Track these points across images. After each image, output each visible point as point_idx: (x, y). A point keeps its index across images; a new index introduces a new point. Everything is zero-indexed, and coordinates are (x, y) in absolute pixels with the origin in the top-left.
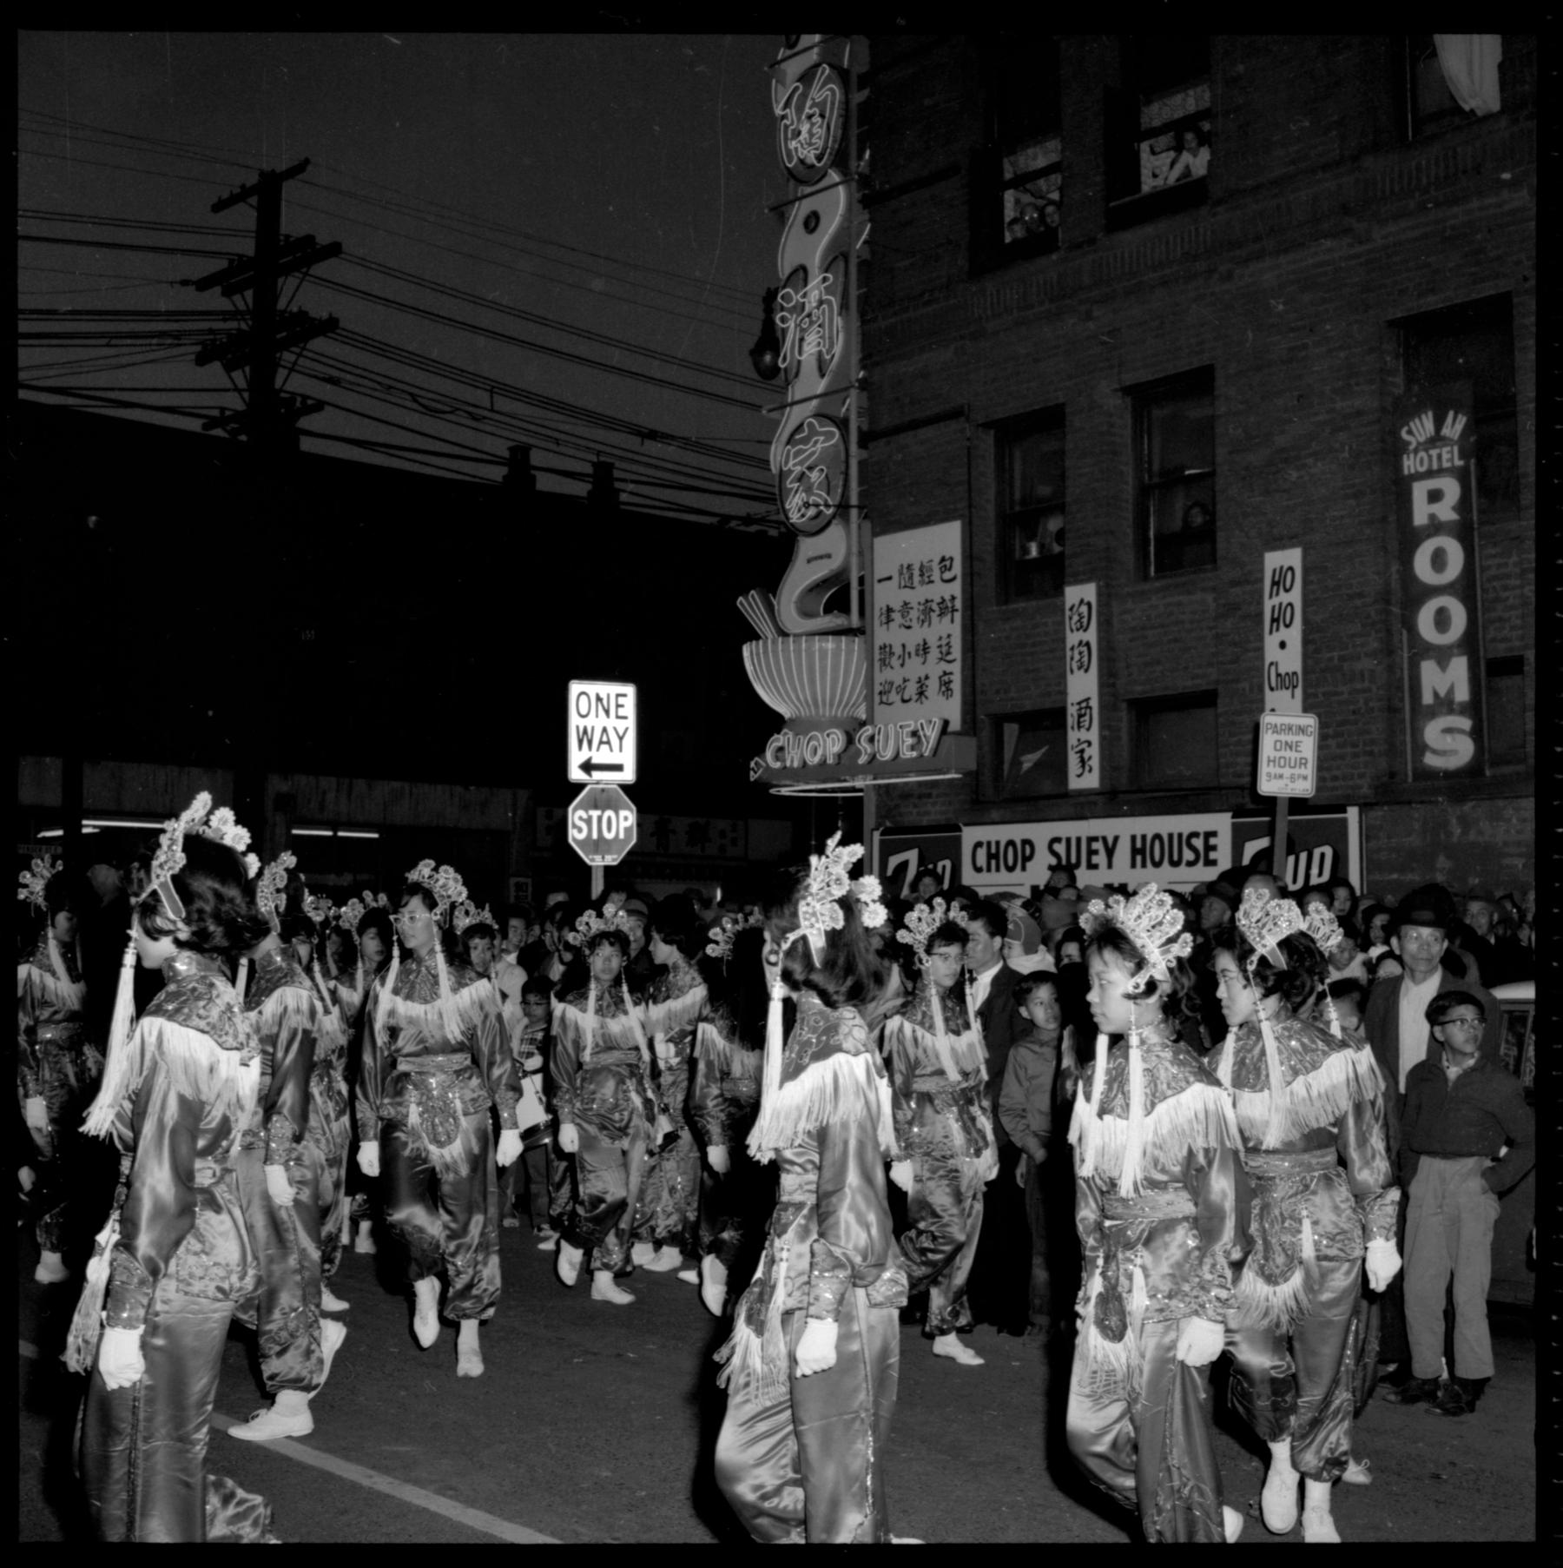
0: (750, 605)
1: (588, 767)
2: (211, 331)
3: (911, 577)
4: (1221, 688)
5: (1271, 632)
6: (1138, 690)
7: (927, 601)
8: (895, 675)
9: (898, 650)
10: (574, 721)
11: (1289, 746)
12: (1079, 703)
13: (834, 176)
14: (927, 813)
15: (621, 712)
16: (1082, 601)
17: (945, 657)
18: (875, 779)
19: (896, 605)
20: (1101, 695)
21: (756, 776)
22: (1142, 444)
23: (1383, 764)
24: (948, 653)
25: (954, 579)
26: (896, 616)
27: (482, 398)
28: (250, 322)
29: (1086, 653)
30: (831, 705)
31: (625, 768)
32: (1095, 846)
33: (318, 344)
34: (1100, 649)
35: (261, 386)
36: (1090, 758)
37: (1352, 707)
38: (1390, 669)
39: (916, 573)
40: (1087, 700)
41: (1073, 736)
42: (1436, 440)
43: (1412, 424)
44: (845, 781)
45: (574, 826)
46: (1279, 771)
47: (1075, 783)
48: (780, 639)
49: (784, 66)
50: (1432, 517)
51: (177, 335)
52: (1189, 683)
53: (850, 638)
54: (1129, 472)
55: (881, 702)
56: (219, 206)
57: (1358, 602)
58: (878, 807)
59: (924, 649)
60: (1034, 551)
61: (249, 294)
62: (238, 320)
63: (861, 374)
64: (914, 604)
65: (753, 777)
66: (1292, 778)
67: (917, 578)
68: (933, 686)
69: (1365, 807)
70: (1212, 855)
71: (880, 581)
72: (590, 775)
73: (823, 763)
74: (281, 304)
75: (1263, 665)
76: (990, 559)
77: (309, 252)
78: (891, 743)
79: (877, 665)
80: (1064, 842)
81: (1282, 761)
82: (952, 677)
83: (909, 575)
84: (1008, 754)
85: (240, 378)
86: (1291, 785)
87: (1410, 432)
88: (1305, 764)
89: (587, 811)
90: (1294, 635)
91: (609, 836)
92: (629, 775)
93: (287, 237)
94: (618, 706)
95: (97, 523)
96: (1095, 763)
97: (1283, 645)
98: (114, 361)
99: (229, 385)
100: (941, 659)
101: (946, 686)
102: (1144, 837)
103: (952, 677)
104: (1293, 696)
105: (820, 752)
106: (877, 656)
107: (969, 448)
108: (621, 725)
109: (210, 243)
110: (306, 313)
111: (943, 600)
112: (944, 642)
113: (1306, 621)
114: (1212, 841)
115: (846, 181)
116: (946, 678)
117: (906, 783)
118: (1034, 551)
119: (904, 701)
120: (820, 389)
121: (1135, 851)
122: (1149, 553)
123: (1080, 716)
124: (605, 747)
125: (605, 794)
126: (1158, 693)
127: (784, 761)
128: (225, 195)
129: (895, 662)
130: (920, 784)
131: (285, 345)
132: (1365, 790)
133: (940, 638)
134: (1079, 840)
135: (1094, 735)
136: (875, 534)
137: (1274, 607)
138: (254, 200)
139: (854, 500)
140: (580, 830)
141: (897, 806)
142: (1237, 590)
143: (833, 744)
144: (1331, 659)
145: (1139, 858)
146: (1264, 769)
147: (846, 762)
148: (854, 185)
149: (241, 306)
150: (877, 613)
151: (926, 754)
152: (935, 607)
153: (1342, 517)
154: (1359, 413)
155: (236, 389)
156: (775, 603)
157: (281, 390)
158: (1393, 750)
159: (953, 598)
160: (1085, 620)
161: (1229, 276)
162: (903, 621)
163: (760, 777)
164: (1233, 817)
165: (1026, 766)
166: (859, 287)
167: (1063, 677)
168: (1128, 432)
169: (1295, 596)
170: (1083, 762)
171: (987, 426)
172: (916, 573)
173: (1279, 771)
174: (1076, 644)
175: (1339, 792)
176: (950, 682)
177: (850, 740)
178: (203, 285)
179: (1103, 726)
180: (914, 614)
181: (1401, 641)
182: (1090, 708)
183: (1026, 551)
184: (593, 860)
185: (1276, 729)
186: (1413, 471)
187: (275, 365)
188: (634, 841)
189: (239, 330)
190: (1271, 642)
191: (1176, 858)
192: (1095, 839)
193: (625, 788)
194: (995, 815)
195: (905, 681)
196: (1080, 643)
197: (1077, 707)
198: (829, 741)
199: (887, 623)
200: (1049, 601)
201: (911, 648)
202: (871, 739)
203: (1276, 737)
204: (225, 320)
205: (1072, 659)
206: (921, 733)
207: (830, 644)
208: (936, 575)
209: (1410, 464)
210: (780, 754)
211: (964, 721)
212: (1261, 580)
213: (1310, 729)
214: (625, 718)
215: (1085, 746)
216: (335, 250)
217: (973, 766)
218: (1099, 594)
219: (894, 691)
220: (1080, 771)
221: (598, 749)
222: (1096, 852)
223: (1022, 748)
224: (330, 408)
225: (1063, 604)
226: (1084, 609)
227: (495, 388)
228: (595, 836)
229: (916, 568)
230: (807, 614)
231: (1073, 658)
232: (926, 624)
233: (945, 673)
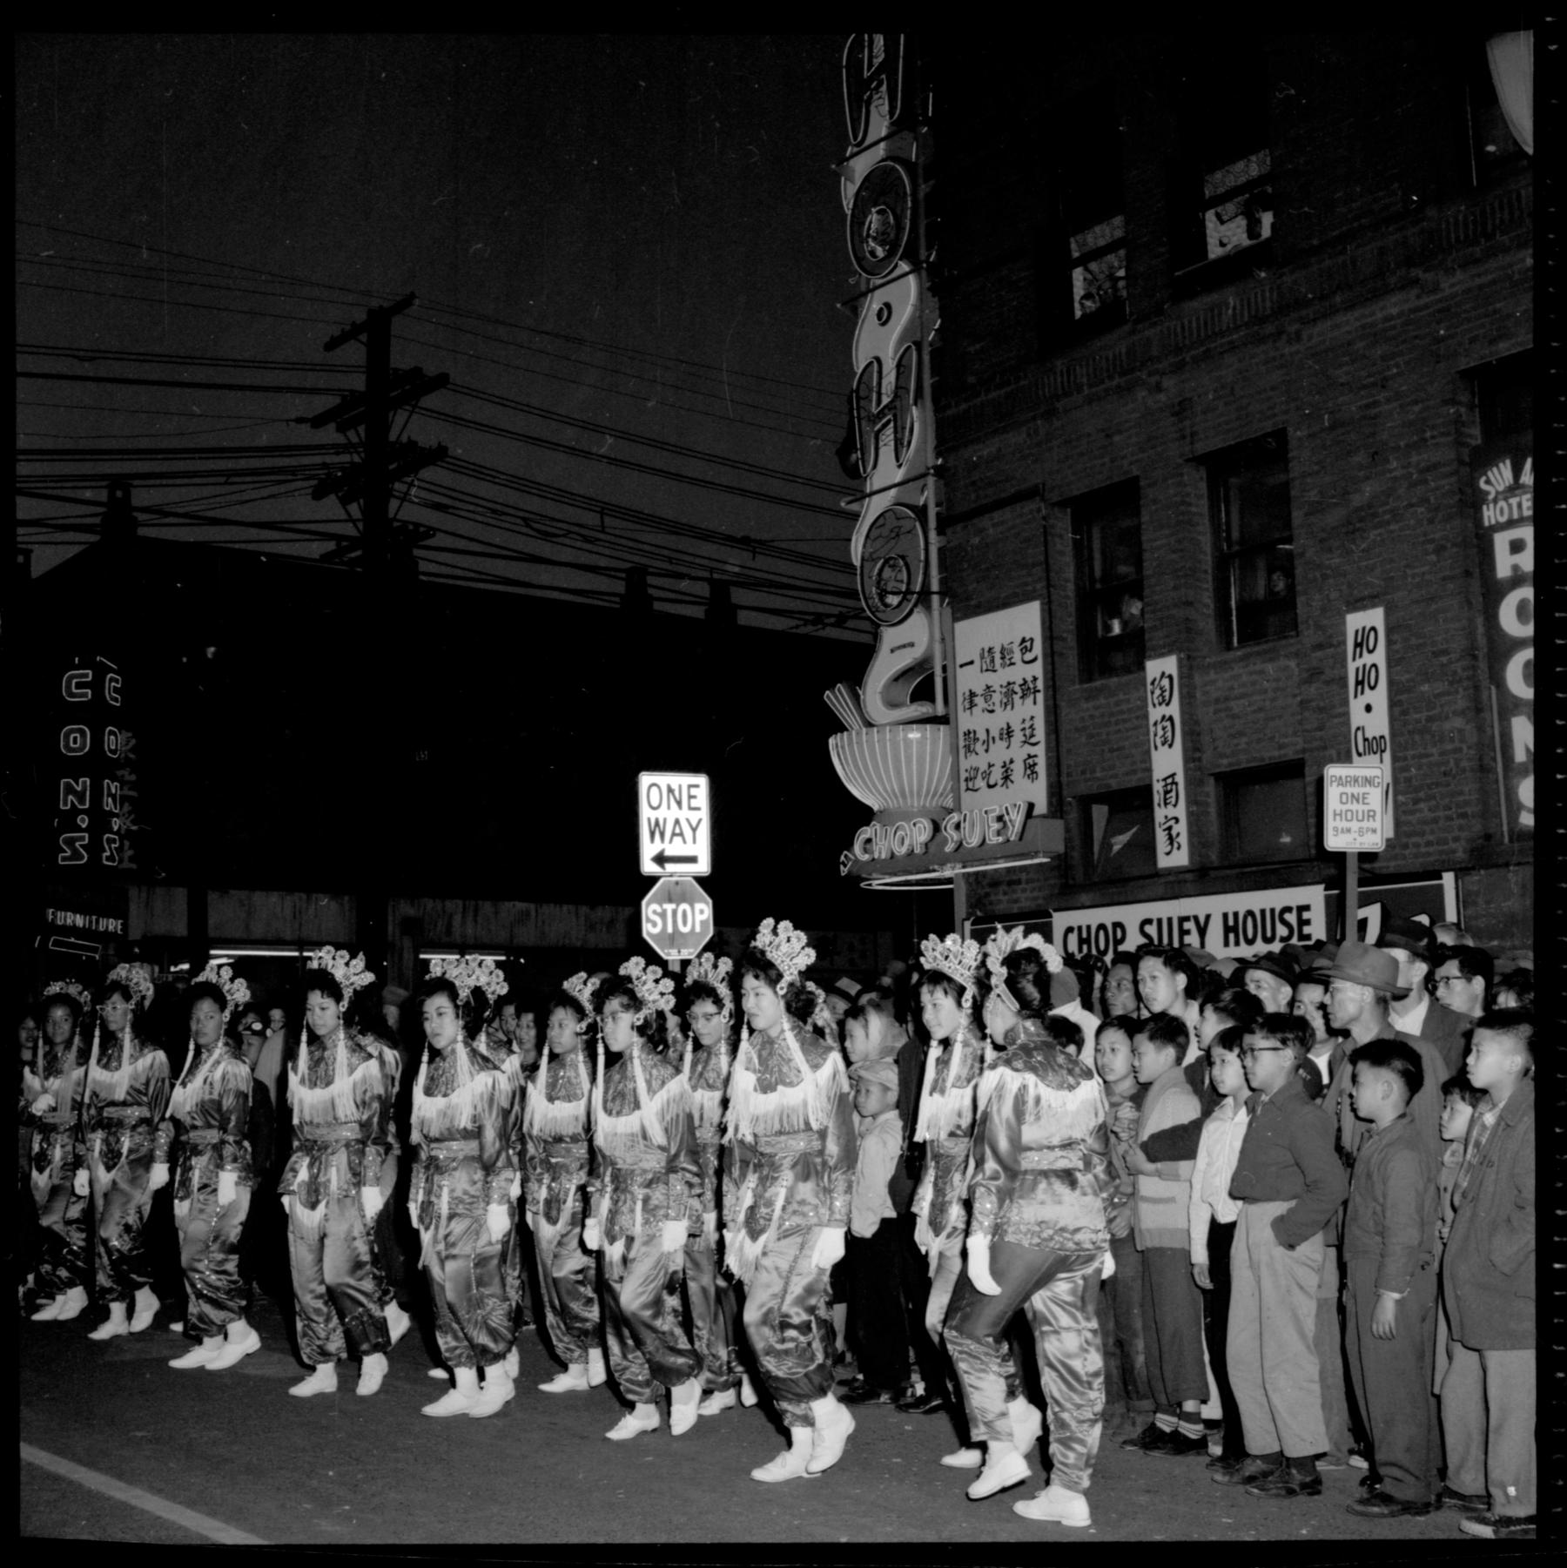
0: (837, 699)
1: (660, 859)
2: (324, 465)
3: (993, 661)
4: (1307, 756)
5: (1356, 696)
6: (1224, 765)
7: (1009, 684)
8: (980, 761)
9: (982, 736)
10: (646, 814)
11: (1355, 798)
12: (1165, 780)
13: (904, 267)
14: (1016, 901)
15: (694, 803)
16: (1163, 674)
17: (1028, 740)
18: (964, 867)
19: (979, 690)
20: (1186, 770)
21: (846, 870)
22: (1220, 511)
23: (1477, 827)
24: (1032, 736)
25: (1035, 660)
26: (979, 700)
27: (592, 519)
28: (363, 455)
29: (1169, 728)
30: (919, 795)
31: (700, 859)
32: (1187, 925)
33: (427, 473)
34: (1183, 723)
35: (375, 515)
36: (1178, 835)
37: (1443, 769)
38: (1480, 729)
39: (997, 656)
40: (1173, 775)
41: (1160, 814)
42: (1515, 488)
43: (1490, 474)
44: (934, 871)
45: (648, 920)
46: (1345, 824)
47: (1164, 862)
48: (864, 730)
49: (852, 162)
50: (1515, 568)
51: (293, 471)
52: (1276, 753)
53: (936, 726)
54: (1206, 541)
55: (968, 789)
56: (332, 345)
57: (1444, 659)
58: (968, 897)
59: (1008, 733)
60: (1117, 628)
61: (362, 429)
62: (351, 453)
63: (940, 461)
64: (996, 687)
65: (844, 871)
66: (1361, 832)
67: (998, 661)
68: (1018, 769)
69: (1461, 872)
70: (1306, 930)
71: (961, 666)
72: (663, 867)
73: (911, 853)
74: (393, 437)
75: (1350, 731)
76: (1071, 640)
77: (418, 385)
78: (978, 830)
79: (962, 751)
80: (1155, 923)
81: (1349, 814)
82: (1036, 760)
83: (992, 658)
84: (1098, 834)
85: (354, 509)
86: (1360, 839)
87: (1488, 482)
88: (1374, 817)
89: (660, 904)
90: (1379, 697)
91: (685, 930)
92: (703, 867)
93: (396, 370)
94: (691, 797)
95: (215, 654)
96: (1183, 840)
97: (1368, 708)
98: (234, 498)
99: (344, 516)
100: (1025, 742)
101: (1030, 769)
102: (1236, 915)
103: (1036, 760)
104: (1381, 761)
105: (907, 842)
106: (962, 743)
107: (1045, 527)
108: (694, 817)
109: (322, 380)
110: (416, 443)
111: (1025, 682)
112: (1027, 725)
113: (1391, 683)
114: (1306, 915)
115: (916, 269)
116: (1031, 761)
117: (996, 870)
118: (1117, 628)
119: (990, 786)
120: (899, 475)
121: (1227, 930)
122: (1231, 621)
123: (1166, 792)
124: (677, 840)
125: (679, 888)
126: (1244, 766)
127: (872, 853)
128: (337, 333)
129: (979, 747)
130: (1009, 870)
131: (398, 476)
132: (1460, 855)
133: (1024, 721)
134: (1170, 920)
135: (1181, 811)
136: (956, 619)
137: (1357, 669)
138: (364, 337)
139: (935, 586)
140: (655, 924)
141: (987, 895)
142: (1319, 654)
143: (919, 834)
144: (1418, 721)
145: (1232, 936)
146: (1330, 823)
147: (931, 853)
148: (924, 273)
149: (355, 440)
150: (960, 699)
151: (1012, 839)
152: (1017, 689)
153: (1424, 574)
154: (1435, 466)
155: (350, 519)
156: (860, 692)
157: (395, 519)
158: (1487, 811)
159: (1035, 679)
160: (1167, 694)
161: (1298, 337)
162: (986, 706)
163: (849, 872)
164: (1326, 889)
165: (1116, 848)
166: (932, 377)
167: (1148, 753)
168: (1205, 502)
169: (1379, 657)
170: (1171, 839)
171: (1062, 504)
172: (997, 656)
173: (1345, 824)
174: (1159, 719)
175: (1432, 859)
176: (1035, 764)
177: (936, 828)
178: (318, 422)
179: (1190, 802)
180: (997, 698)
181: (1490, 697)
182: (1176, 784)
183: (1108, 628)
184: (669, 954)
185: (1341, 782)
186: (1493, 522)
187: (390, 494)
188: (711, 934)
189: (352, 463)
190: (1356, 706)
191: (1269, 934)
192: (1187, 919)
193: (700, 880)
194: (1084, 898)
195: (990, 766)
196: (1164, 717)
197: (1163, 783)
198: (915, 830)
199: (970, 708)
200: (1131, 677)
201: (995, 733)
202: (958, 827)
203: (1341, 789)
204: (337, 454)
205: (1155, 735)
206: (1006, 818)
207: (914, 734)
208: (1017, 656)
209: (1490, 515)
210: (868, 846)
211: (1050, 804)
212: (1344, 643)
213: (1377, 780)
214: (698, 809)
215: (1172, 822)
216: (442, 381)
217: (1061, 848)
218: (1180, 666)
219: (979, 777)
220: (1169, 848)
221: (671, 841)
222: (1188, 932)
223: (1111, 831)
224: (442, 535)
225: (1144, 679)
226: (1166, 682)
227: (605, 509)
228: (670, 930)
229: (997, 650)
230: (892, 705)
231: (1156, 734)
232: (1009, 707)
233: (1030, 756)
